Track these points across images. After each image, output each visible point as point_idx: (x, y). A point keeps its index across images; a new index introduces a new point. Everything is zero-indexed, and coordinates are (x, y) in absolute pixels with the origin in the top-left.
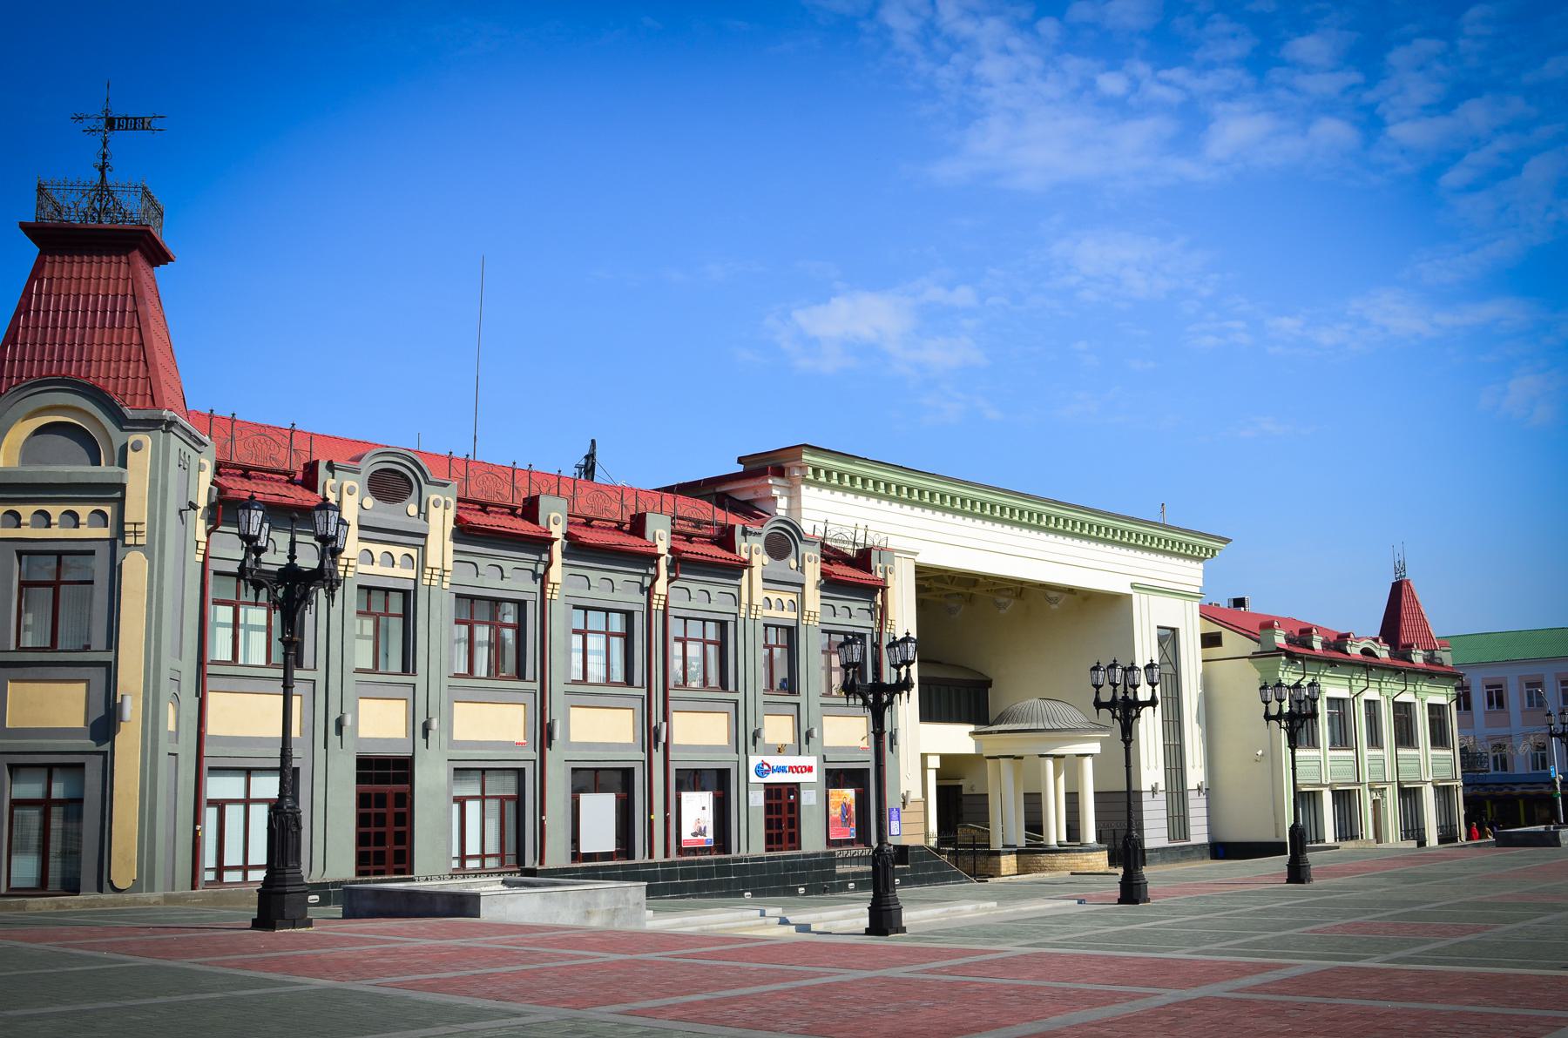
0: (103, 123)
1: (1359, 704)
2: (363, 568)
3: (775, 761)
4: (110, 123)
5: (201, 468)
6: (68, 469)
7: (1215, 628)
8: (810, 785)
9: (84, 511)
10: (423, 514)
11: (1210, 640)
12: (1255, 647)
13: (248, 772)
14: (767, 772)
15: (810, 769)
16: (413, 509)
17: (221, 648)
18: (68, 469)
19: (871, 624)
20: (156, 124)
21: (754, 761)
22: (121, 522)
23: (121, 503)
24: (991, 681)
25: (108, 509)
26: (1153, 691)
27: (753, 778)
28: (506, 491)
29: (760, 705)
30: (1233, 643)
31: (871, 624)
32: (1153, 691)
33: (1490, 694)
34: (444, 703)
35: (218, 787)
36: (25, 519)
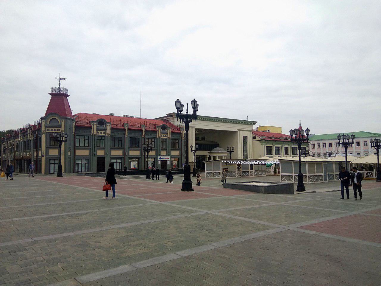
0: (59, 79)
1: (283, 148)
2: (97, 134)
3: (162, 157)
4: (60, 79)
5: (73, 123)
6: (54, 124)
7: (255, 136)
8: (168, 160)
9: (102, 132)
10: (106, 127)
11: (254, 138)
12: (260, 139)
13: (54, 160)
14: (161, 159)
15: (168, 158)
16: (104, 126)
17: (78, 145)
18: (54, 124)
19: (123, 135)
20: (66, 79)
21: (159, 157)
22: (106, 133)
23: (167, 135)
24: (219, 144)
25: (105, 132)
26: (371, 144)
27: (159, 159)
28: (119, 123)
29: (160, 149)
30: (258, 138)
31: (123, 135)
32: (371, 144)
33: (365, 144)
34: (96, 150)
35: (77, 162)
36: (50, 130)
